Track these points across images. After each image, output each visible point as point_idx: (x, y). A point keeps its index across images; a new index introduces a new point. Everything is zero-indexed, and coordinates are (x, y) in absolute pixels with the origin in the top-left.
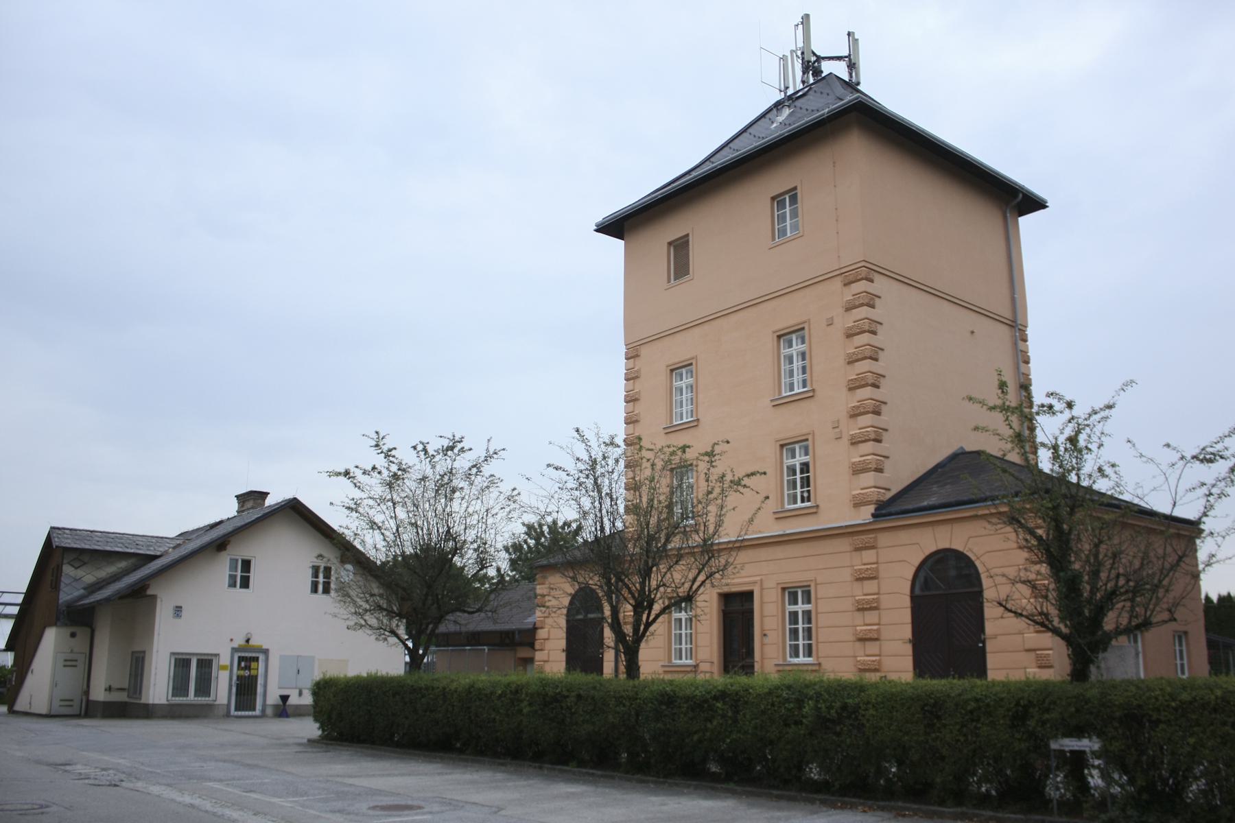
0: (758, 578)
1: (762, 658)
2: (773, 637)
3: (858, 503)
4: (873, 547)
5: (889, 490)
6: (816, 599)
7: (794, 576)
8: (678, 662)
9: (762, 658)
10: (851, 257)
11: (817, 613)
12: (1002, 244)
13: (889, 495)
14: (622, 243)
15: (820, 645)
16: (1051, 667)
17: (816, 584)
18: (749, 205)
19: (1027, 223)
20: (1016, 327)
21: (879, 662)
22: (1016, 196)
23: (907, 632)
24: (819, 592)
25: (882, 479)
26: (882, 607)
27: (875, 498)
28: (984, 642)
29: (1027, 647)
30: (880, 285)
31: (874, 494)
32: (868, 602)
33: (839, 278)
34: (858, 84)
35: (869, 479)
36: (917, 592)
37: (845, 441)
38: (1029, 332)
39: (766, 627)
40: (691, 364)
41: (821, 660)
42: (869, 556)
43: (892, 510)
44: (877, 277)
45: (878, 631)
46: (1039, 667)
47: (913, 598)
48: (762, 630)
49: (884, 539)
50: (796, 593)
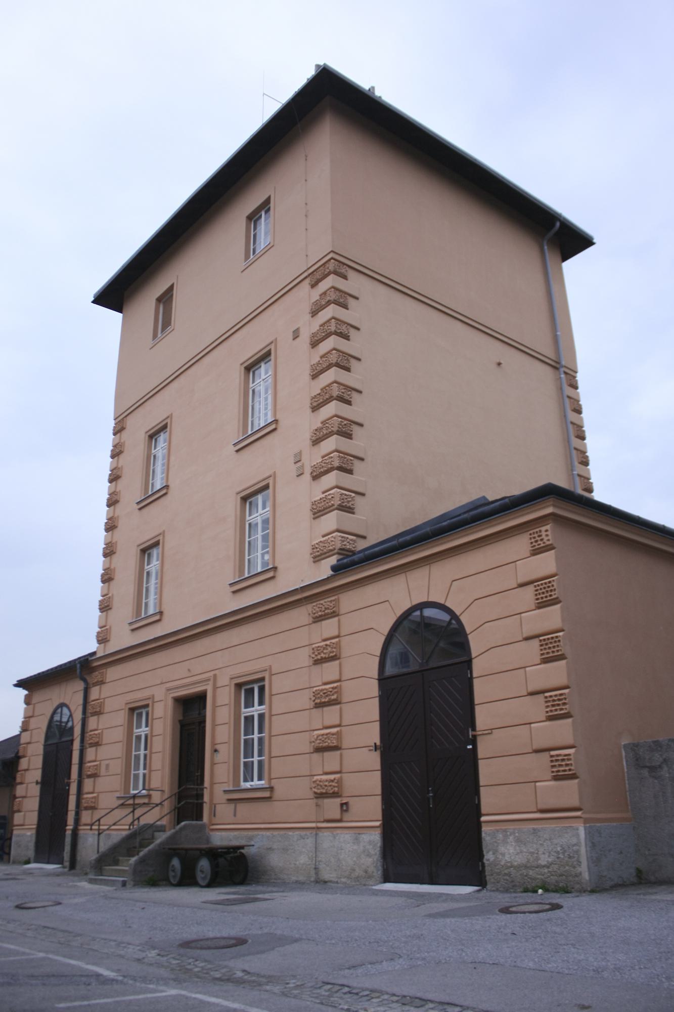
0: (212, 674)
1: (212, 784)
2: (225, 753)
3: (318, 557)
4: (334, 614)
5: (364, 537)
6: (271, 695)
7: (247, 669)
8: (248, 785)
9: (212, 784)
10: (319, 249)
11: (271, 715)
12: (539, 277)
13: (361, 545)
14: (118, 316)
15: (153, 755)
16: (573, 777)
17: (271, 675)
18: (226, 235)
19: (574, 269)
20: (562, 370)
21: (340, 782)
22: (553, 225)
23: (374, 734)
24: (276, 685)
25: (350, 522)
26: (344, 700)
27: (339, 545)
28: (474, 742)
29: (536, 746)
30: (354, 284)
31: (337, 542)
32: (326, 693)
33: (307, 281)
34: (590, 490)
35: (331, 521)
36: (390, 670)
37: (307, 477)
38: (580, 377)
39: (218, 740)
40: (266, 487)
41: (274, 783)
42: (329, 627)
43: (356, 563)
44: (351, 274)
45: (339, 734)
46: (556, 778)
47: (383, 680)
48: (214, 744)
49: (348, 601)
50: (252, 690)
